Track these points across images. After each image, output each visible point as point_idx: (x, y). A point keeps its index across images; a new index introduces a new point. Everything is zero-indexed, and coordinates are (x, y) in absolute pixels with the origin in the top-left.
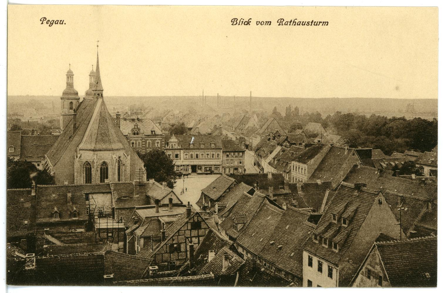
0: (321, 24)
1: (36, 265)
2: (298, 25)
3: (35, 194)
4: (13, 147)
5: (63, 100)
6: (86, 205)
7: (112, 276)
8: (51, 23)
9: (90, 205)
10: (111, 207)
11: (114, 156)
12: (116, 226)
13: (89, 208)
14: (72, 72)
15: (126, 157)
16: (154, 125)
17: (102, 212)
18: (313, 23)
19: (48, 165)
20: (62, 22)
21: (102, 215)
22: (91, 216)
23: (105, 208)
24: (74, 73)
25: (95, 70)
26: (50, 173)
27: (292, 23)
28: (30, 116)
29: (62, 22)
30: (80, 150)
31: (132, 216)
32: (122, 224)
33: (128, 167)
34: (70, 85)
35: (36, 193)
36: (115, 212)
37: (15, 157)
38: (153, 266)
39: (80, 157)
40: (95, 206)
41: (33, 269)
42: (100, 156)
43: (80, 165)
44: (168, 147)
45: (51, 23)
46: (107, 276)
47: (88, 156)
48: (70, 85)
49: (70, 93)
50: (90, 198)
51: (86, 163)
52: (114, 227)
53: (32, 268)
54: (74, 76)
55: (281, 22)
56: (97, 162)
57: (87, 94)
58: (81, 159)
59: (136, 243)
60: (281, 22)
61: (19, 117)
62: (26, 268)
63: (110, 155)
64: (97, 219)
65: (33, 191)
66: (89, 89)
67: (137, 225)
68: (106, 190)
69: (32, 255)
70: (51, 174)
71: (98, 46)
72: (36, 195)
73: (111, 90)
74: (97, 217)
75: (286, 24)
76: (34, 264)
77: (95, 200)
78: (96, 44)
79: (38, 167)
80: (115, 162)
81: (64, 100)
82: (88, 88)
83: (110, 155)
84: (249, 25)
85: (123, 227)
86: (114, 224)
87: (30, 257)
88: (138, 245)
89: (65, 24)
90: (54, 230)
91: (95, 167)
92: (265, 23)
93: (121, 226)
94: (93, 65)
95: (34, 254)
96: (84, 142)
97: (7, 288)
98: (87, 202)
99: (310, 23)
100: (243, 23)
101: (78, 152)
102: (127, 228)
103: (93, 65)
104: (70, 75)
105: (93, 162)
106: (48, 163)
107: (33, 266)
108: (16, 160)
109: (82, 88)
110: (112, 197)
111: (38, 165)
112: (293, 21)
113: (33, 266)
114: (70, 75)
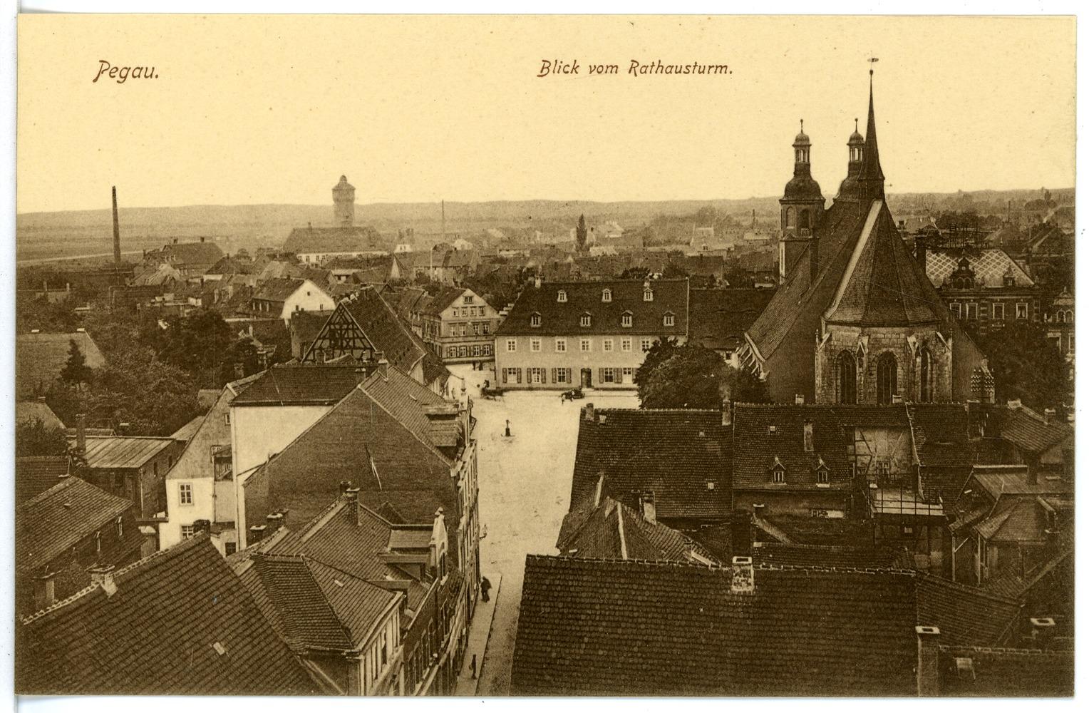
0: (713, 70)
1: (755, 584)
2: (676, 73)
3: (730, 423)
4: (630, 315)
5: (577, 221)
6: (848, 455)
7: (936, 630)
8: (122, 75)
9: (856, 456)
10: (909, 465)
11: (911, 340)
12: (923, 510)
13: (856, 462)
14: (808, 139)
15: (941, 341)
16: (1013, 263)
17: (886, 475)
18: (697, 68)
19: (751, 357)
20: (151, 75)
21: (888, 483)
22: (861, 482)
23: (893, 464)
24: (811, 142)
25: (863, 132)
26: (759, 375)
27: (655, 68)
28: (704, 245)
29: (95, 81)
30: (829, 322)
31: (964, 490)
32: (937, 507)
33: (946, 368)
34: (802, 170)
35: (732, 422)
36: (920, 477)
37: (678, 338)
38: (928, 625)
39: (830, 339)
40: (869, 458)
41: (750, 592)
42: (876, 339)
43: (829, 359)
44: (1050, 320)
45: (122, 75)
46: (925, 630)
47: (849, 337)
48: (802, 170)
49: (802, 187)
50: (857, 439)
51: (843, 355)
52: (919, 512)
53: (745, 589)
54: (811, 148)
55: (634, 67)
56: (869, 354)
57: (843, 189)
58: (831, 345)
59: (978, 556)
60: (634, 67)
61: (680, 248)
62: (734, 589)
63: (903, 336)
64: (875, 489)
65: (725, 415)
66: (849, 176)
67: (978, 513)
68: (890, 420)
69: (747, 560)
70: (761, 378)
71: (871, 72)
72: (731, 426)
73: (904, 178)
74: (875, 486)
75: (643, 71)
76: (751, 580)
77: (869, 443)
78: (869, 66)
79: (727, 361)
80: (914, 352)
81: (788, 206)
82: (791, 176)
83: (903, 336)
84: (577, 73)
85: (940, 513)
86: (919, 505)
87: (743, 565)
88: (982, 561)
89: (157, 76)
90: (776, 510)
91: (865, 365)
92: (605, 68)
93: (937, 511)
94: (856, 120)
95: (750, 559)
96: (836, 306)
97: (17, 701)
98: (851, 447)
99: (691, 69)
100: (562, 67)
101: (824, 329)
102: (953, 520)
103: (856, 120)
104: (802, 145)
105: (861, 354)
106: (751, 352)
107: (749, 584)
108: (680, 344)
109: (831, 175)
110: (911, 439)
111: (728, 357)
112: (656, 64)
113: (749, 584)
114: (802, 145)
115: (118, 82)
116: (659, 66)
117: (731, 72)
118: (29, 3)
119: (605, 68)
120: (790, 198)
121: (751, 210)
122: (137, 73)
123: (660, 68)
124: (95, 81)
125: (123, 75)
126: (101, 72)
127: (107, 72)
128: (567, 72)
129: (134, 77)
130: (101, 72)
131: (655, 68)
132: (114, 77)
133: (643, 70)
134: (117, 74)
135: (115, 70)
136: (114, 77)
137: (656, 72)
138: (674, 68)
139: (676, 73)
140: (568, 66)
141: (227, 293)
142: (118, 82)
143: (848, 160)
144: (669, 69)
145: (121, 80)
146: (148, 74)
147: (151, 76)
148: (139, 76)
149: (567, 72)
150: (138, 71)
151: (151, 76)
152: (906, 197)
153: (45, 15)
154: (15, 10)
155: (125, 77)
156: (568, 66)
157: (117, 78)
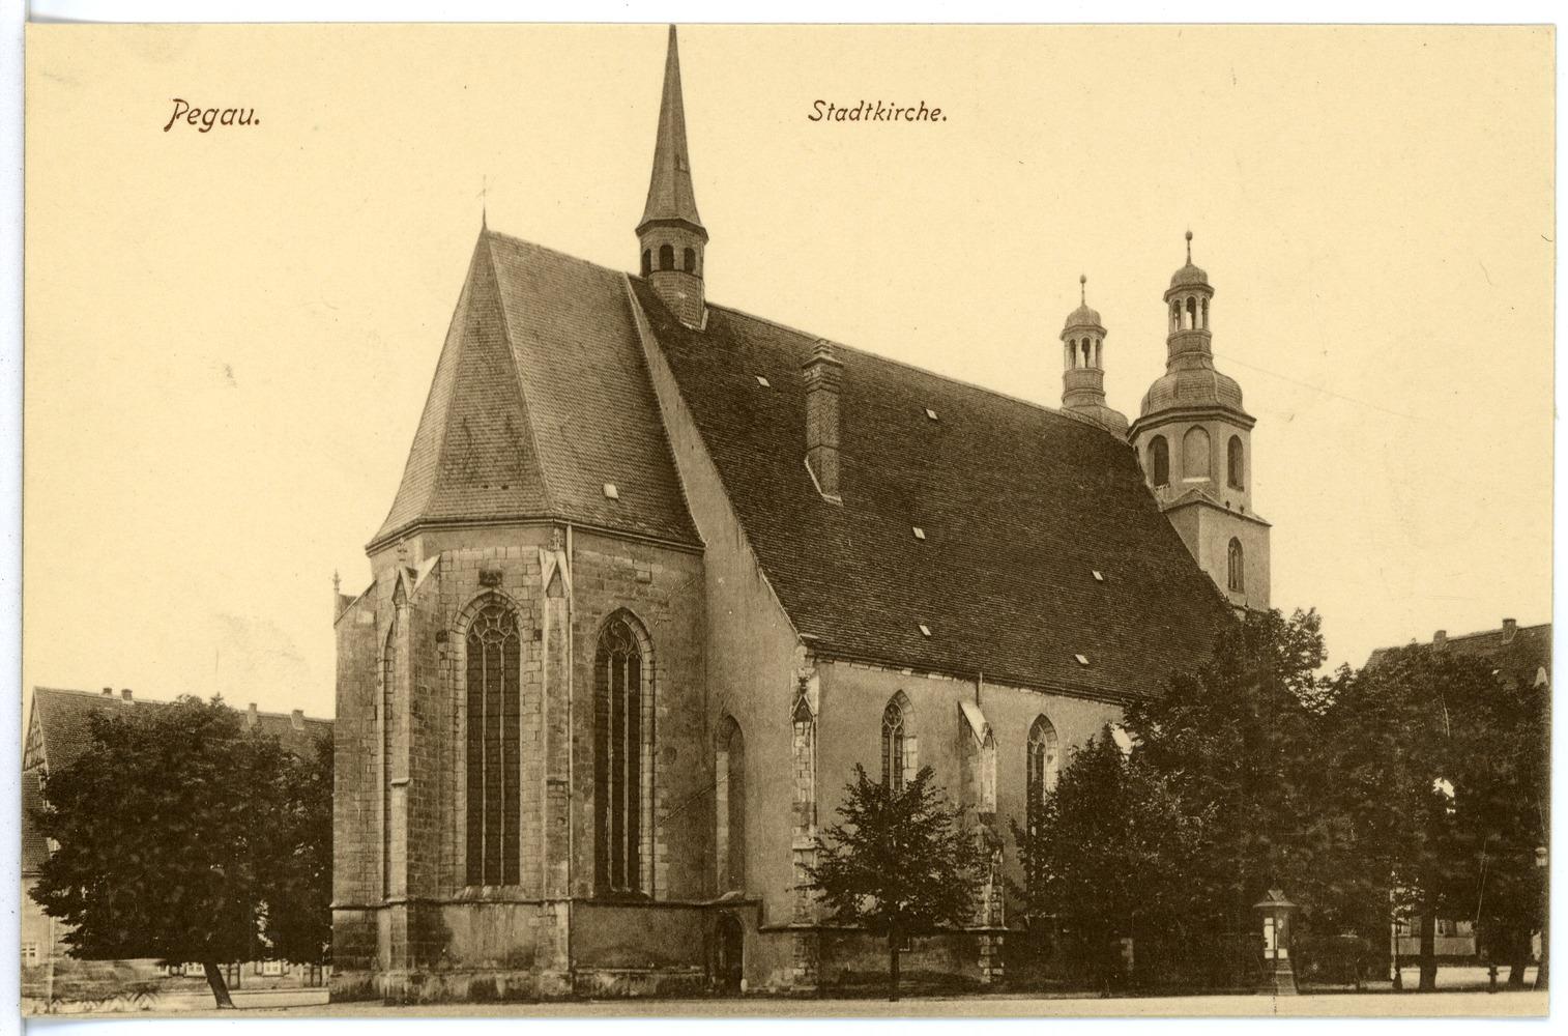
8: (204, 120)
18: (834, 113)
27: (872, 113)
29: (167, 128)
45: (204, 120)
89: (257, 122)
112: (875, 106)
115: (201, 130)
116: (922, 110)
117: (945, 119)
118: (42, 8)
119: (847, 116)
120: (1320, 914)
121: (1441, 966)
122: (228, 117)
123: (924, 113)
124: (167, 128)
125: (208, 120)
126: (176, 116)
127: (186, 116)
128: (911, 119)
129: (223, 123)
130: (176, 116)
131: (872, 113)
132: (195, 123)
133: (840, 115)
134: (199, 119)
135: (196, 113)
136: (195, 123)
137: (925, 119)
138: (238, 115)
139: (241, 123)
140: (913, 110)
141: (1348, 710)
142: (201, 130)
143: (1166, 334)
144: (841, 113)
145: (205, 127)
146: (244, 119)
147: (249, 121)
148: (231, 122)
149: (911, 119)
150: (841, 113)
151: (249, 121)
152: (1545, 707)
153: (67, 26)
154: (19, 15)
155: (211, 124)
156: (913, 110)
157: (200, 124)
